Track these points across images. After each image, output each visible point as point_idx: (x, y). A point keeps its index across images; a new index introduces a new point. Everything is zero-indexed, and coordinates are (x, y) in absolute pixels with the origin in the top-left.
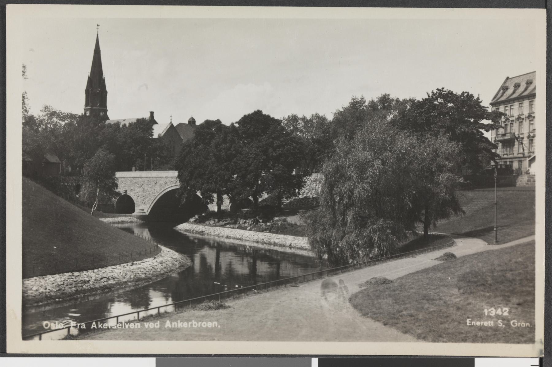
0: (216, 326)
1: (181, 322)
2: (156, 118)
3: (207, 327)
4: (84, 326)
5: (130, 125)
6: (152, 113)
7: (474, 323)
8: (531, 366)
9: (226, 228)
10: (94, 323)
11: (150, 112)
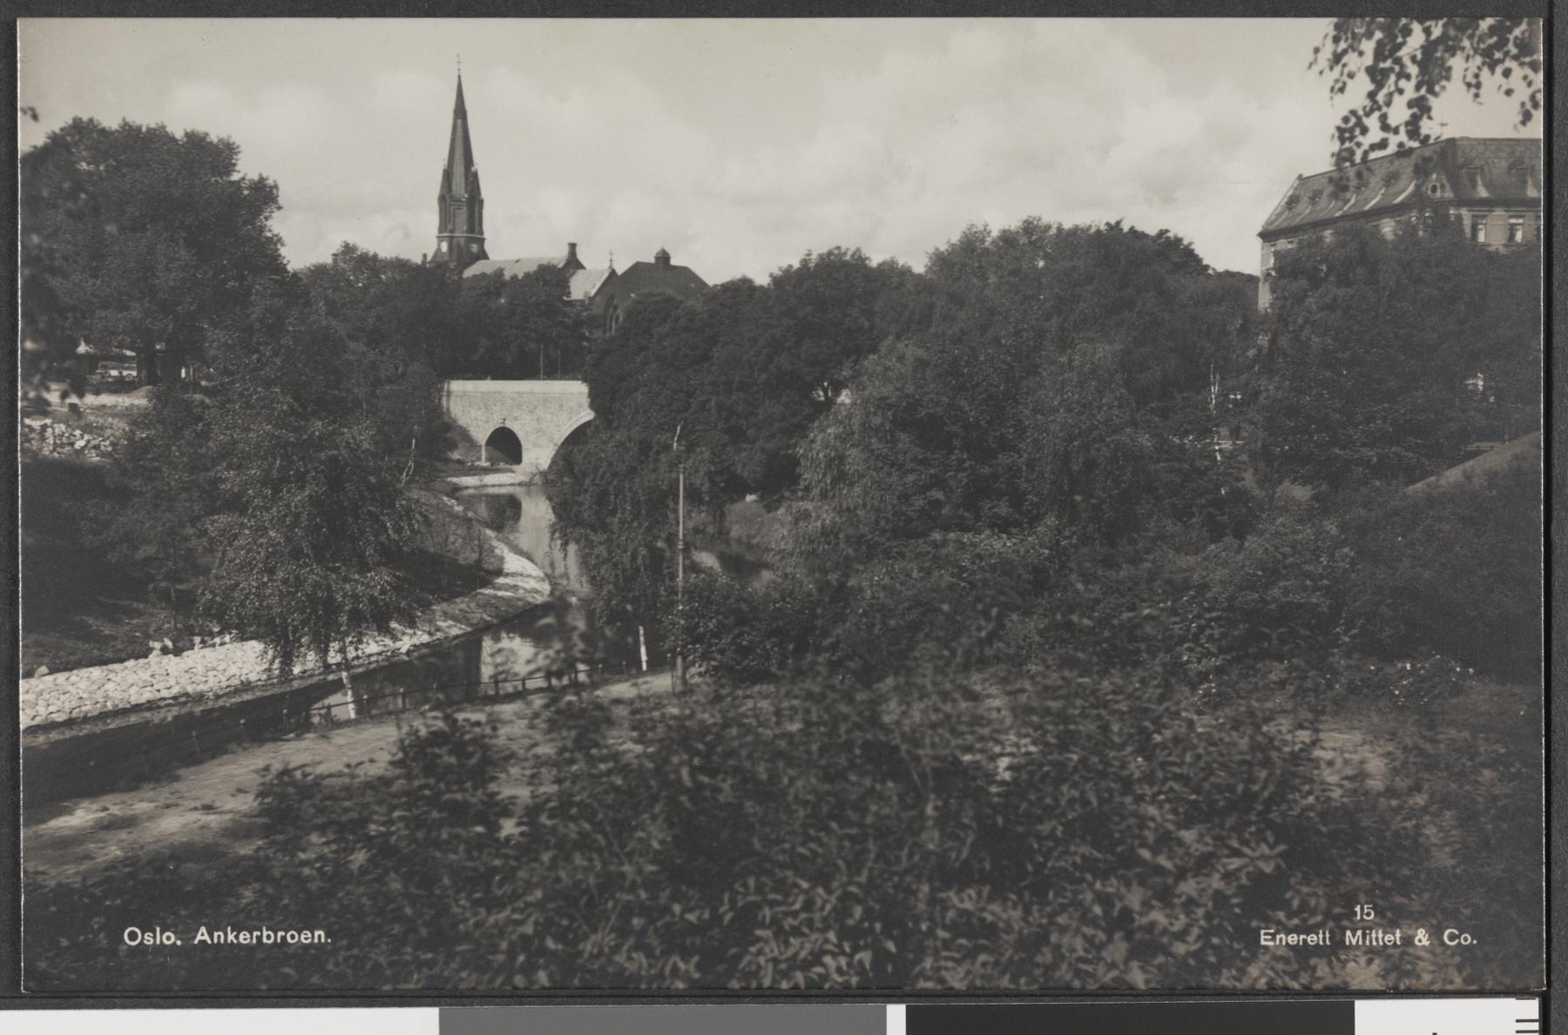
2: (581, 257)
5: (527, 275)
6: (573, 246)
9: (231, 812)
10: (203, 929)
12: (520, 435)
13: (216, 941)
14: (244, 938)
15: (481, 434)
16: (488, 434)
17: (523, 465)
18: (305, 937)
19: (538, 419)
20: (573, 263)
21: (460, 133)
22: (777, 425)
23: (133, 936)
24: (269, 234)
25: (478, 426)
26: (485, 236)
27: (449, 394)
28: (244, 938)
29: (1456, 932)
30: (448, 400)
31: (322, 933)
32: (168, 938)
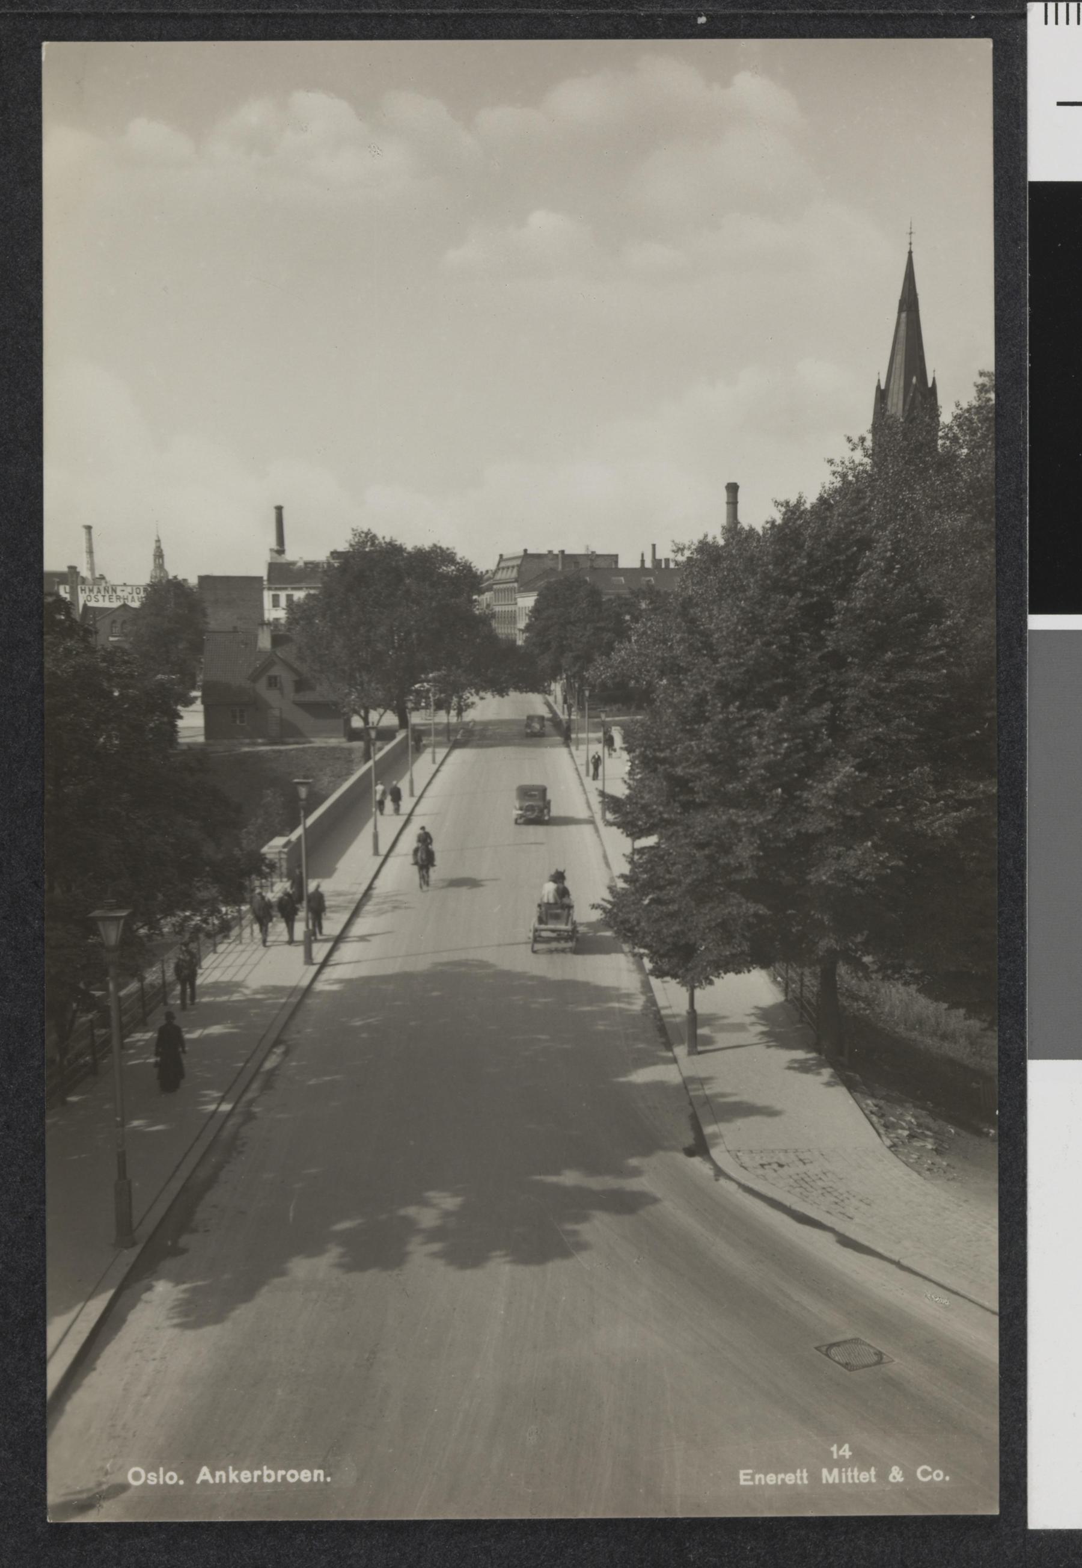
0: (322, 1479)
1: (234, 1470)
3: (299, 1480)
4: (742, 1477)
7: (760, 1479)
8: (1059, 104)
11: (616, 556)
14: (246, 1476)
18: (305, 1476)
21: (908, 338)
24: (247, 883)
29: (929, 1469)
31: (321, 1472)
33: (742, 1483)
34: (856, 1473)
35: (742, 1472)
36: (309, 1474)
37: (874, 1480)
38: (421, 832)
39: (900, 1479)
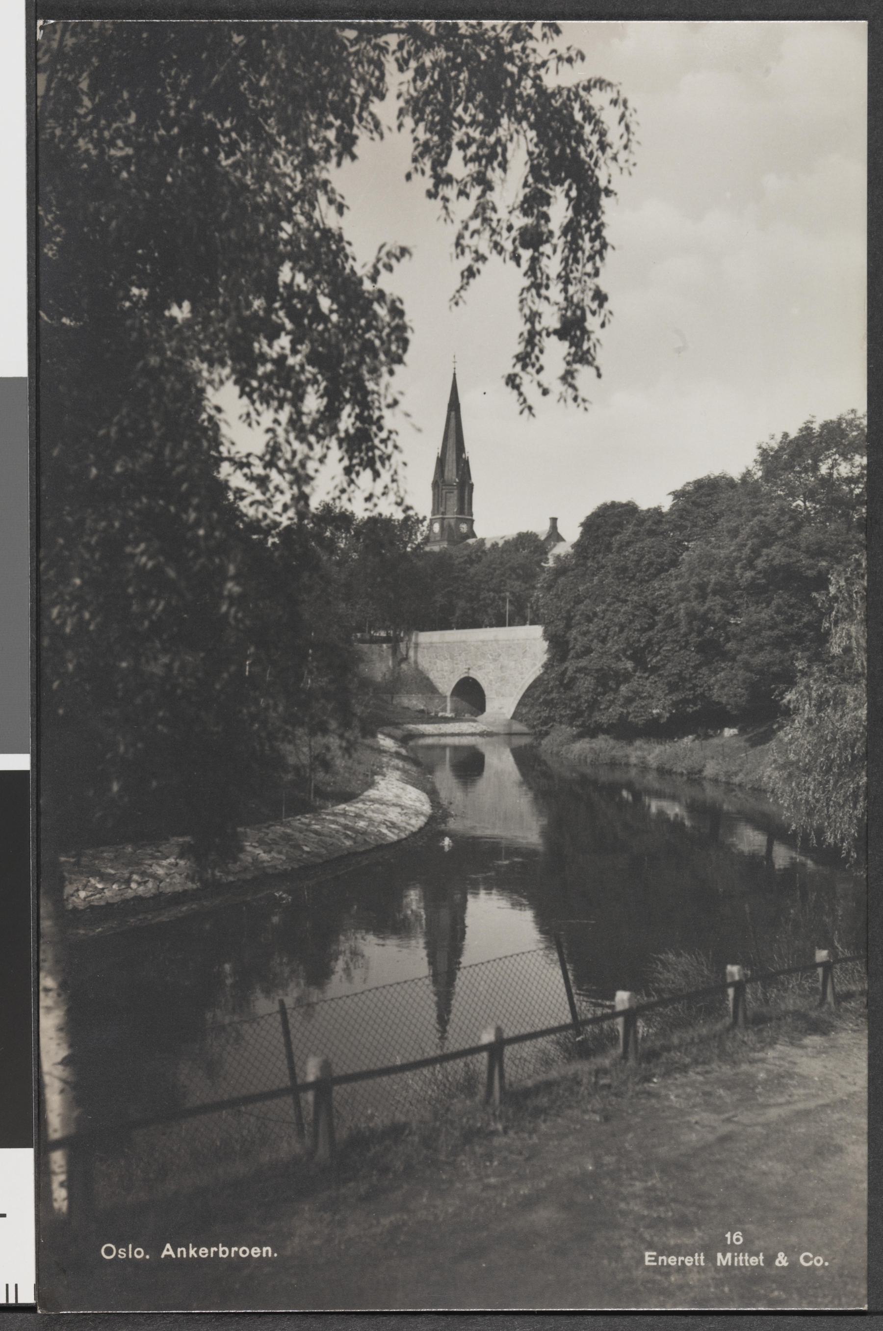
0: (270, 1255)
4: (647, 1259)
6: (554, 521)
7: (663, 1260)
10: (168, 1246)
12: (484, 684)
13: (179, 1256)
14: (204, 1252)
15: (446, 684)
16: (453, 685)
17: (485, 714)
19: (502, 667)
20: (555, 535)
22: (767, 633)
23: (109, 1251)
25: (443, 677)
26: (474, 517)
27: (417, 645)
28: (204, 1252)
29: (811, 1255)
30: (416, 652)
32: (139, 1253)
33: (647, 1263)
34: (746, 1258)
35: (647, 1254)
36: (259, 1251)
37: (762, 1264)
38: (760, 451)
39: (785, 1263)
